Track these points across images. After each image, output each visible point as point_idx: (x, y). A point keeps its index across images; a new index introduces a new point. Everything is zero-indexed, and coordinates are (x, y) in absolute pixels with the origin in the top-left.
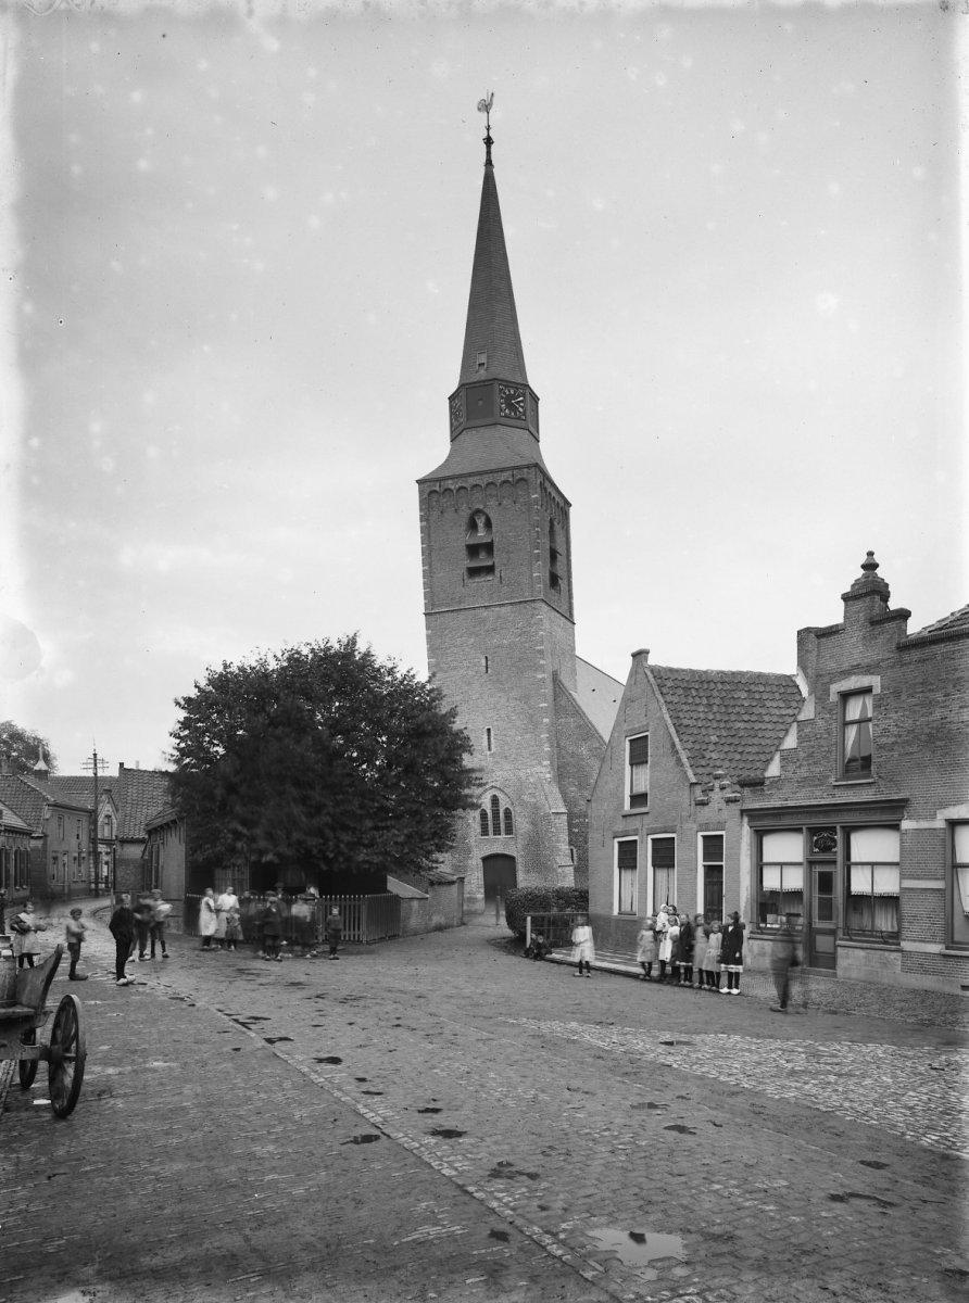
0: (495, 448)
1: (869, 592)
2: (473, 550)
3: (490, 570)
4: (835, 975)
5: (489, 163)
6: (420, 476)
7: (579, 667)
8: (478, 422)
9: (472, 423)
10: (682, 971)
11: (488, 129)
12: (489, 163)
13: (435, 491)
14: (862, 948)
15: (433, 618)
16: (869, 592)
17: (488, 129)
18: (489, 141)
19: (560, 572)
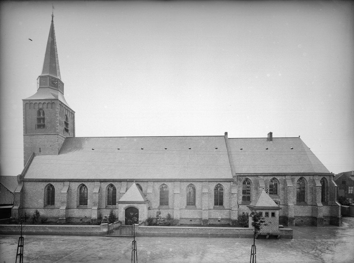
5: (52, 21)
6: (24, 99)
8: (43, 86)
9: (41, 86)
12: (52, 21)
13: (28, 103)
18: (53, 17)
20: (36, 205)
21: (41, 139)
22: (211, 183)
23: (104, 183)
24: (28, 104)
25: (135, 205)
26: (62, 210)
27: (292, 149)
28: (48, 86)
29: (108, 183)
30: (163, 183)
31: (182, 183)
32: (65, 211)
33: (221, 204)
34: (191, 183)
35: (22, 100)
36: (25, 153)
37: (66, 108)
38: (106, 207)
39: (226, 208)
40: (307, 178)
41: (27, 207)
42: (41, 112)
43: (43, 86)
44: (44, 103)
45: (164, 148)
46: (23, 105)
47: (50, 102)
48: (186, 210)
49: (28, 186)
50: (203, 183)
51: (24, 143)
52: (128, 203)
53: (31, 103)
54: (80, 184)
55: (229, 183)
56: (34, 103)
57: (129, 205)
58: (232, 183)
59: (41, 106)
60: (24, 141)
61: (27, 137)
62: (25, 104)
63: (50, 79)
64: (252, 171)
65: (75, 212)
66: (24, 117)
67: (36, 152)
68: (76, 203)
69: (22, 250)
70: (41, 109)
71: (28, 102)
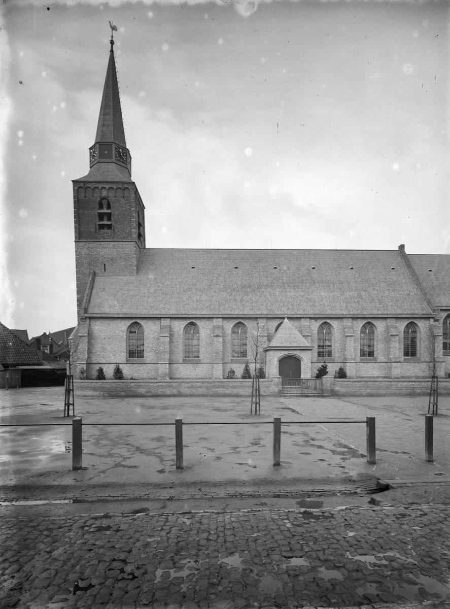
0: (112, 171)
1: (402, 247)
2: (101, 216)
3: (109, 227)
4: (376, 359)
5: (112, 51)
6: (75, 178)
7: (409, 257)
8: (105, 160)
9: (101, 160)
10: (410, 354)
11: (112, 37)
12: (112, 51)
13: (81, 187)
14: (183, 379)
15: (77, 243)
16: (402, 247)
17: (112, 37)
18: (112, 42)
19: (141, 232)
20: (112, 357)
21: (106, 249)
22: (399, 321)
23: (228, 320)
24: (80, 186)
25: (297, 353)
26: (163, 365)
27: (352, 268)
28: (114, 160)
29: (234, 320)
30: (324, 321)
31: (355, 322)
32: (168, 367)
33: (414, 354)
34: (369, 320)
35: (72, 181)
36: (77, 273)
38: (184, 360)
39: (337, 360)
40: (334, 323)
41: (96, 362)
42: (104, 202)
43: (105, 160)
44: (110, 188)
45: (316, 269)
46: (74, 190)
47: (120, 186)
48: (362, 364)
49: (98, 327)
50: (388, 320)
51: (76, 255)
52: (284, 350)
53: (88, 187)
54: (237, 321)
55: (427, 322)
56: (92, 187)
57: (286, 352)
58: (432, 321)
59: (104, 193)
60: (76, 251)
61: (81, 244)
62: (76, 188)
63: (116, 148)
64: (247, 311)
65: (180, 369)
66: (75, 212)
67: (97, 272)
68: (181, 354)
69: (435, 410)
70: (104, 198)
71: (82, 185)
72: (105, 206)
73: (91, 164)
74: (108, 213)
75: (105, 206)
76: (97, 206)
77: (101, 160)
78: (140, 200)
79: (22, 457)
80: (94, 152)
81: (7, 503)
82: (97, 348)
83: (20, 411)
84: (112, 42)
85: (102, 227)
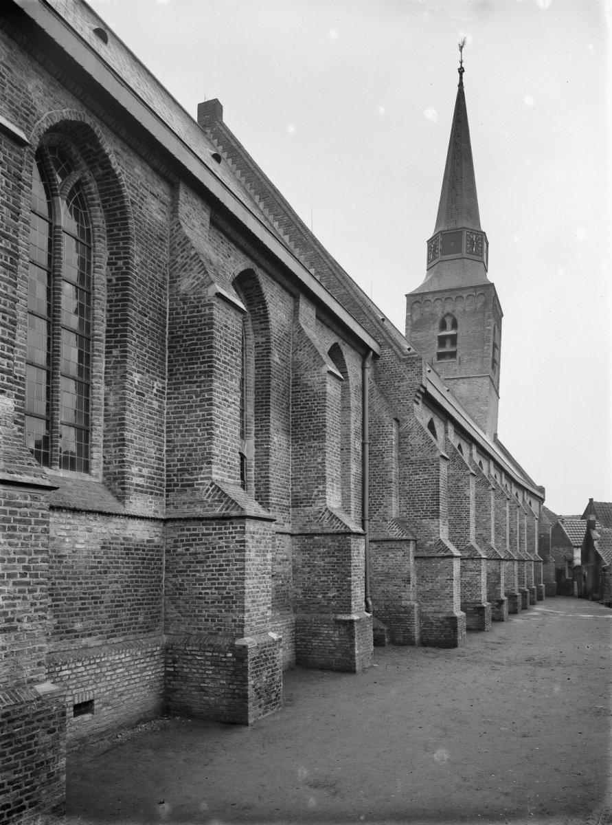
3: (453, 355)
5: (461, 85)
6: (408, 292)
11: (461, 63)
12: (461, 85)
18: (461, 71)
19: (496, 358)
37: (447, 295)
42: (449, 321)
70: (448, 314)
72: (449, 325)
73: (428, 264)
74: (451, 352)
75: (449, 325)
76: (437, 325)
77: (445, 257)
78: (498, 307)
79: (390, 494)
80: (435, 246)
81: (516, 572)
82: (443, 429)
83: (20, 814)
84: (461, 71)
85: (441, 356)
